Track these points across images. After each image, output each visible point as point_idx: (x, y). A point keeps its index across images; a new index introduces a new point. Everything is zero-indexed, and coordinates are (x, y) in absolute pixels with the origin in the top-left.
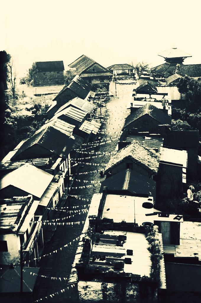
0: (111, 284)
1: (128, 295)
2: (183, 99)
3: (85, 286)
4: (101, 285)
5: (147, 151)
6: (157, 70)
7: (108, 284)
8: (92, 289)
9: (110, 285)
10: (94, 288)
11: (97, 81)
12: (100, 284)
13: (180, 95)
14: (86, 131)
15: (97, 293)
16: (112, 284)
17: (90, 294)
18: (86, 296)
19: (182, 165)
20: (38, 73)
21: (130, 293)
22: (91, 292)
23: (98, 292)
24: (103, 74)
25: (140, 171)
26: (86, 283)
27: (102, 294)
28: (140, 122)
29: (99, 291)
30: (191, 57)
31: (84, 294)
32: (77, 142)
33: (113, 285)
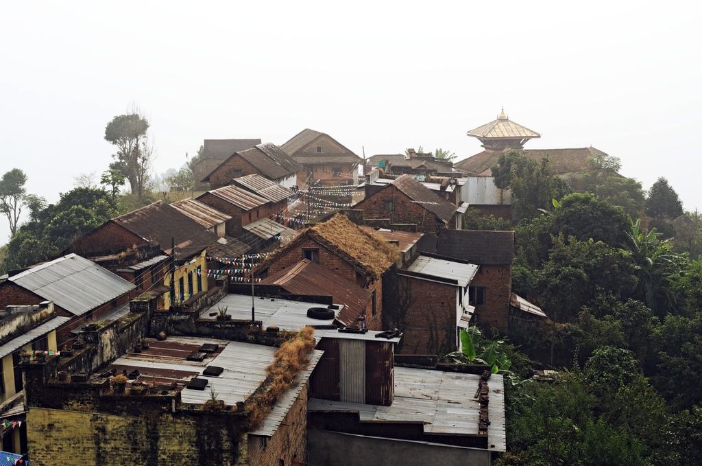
1: (164, 454)
3: (46, 423)
4: (91, 420)
6: (465, 165)
8: (65, 434)
9: (115, 423)
10: (70, 431)
11: (325, 174)
12: (88, 417)
13: (499, 195)
14: (259, 233)
16: (121, 419)
18: (49, 456)
19: (456, 282)
20: (205, 162)
22: (63, 443)
24: (339, 158)
25: (337, 269)
27: (92, 448)
28: (375, 203)
29: (85, 441)
30: (537, 139)
31: (43, 450)
33: (122, 424)
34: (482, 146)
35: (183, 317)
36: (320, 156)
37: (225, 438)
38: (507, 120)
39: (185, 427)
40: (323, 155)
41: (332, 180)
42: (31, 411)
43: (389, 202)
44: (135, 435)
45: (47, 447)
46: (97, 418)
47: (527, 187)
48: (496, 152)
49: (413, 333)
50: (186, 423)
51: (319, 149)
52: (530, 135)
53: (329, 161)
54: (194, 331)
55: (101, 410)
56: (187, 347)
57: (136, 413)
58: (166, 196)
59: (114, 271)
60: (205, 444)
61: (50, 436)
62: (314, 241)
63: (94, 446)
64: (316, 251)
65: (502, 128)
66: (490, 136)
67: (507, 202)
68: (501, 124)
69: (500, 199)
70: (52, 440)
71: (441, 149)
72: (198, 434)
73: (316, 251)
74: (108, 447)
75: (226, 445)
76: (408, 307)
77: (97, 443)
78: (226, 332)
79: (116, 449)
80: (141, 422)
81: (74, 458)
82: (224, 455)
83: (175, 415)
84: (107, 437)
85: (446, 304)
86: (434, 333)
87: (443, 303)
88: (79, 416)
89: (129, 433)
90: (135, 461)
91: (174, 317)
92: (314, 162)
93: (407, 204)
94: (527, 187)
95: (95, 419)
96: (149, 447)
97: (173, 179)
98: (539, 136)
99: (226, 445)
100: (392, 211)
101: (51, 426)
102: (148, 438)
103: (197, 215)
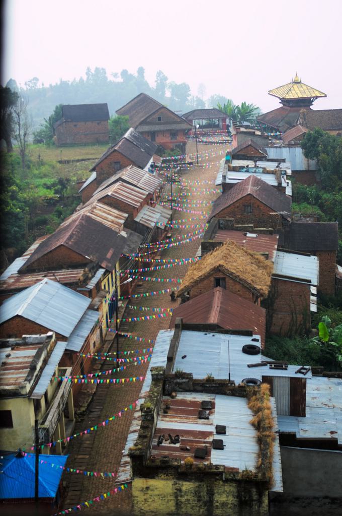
1: (217, 502)
3: (145, 486)
4: (173, 485)
8: (156, 492)
9: (187, 486)
10: (159, 491)
12: (170, 483)
15: (165, 500)
16: (191, 484)
18: (146, 505)
21: (222, 499)
24: (175, 125)
25: (239, 291)
26: (147, 482)
28: (238, 207)
31: (142, 501)
33: (191, 486)
34: (280, 103)
35: (184, 380)
36: (161, 124)
37: (254, 493)
38: (300, 82)
39: (230, 488)
40: (163, 124)
41: (171, 143)
42: (135, 480)
43: (248, 206)
44: (200, 492)
45: (145, 500)
46: (176, 484)
47: (331, 162)
48: (292, 109)
49: (279, 316)
50: (231, 486)
51: (159, 119)
52: (318, 95)
53: (168, 128)
54: (192, 389)
55: (178, 479)
56: (193, 404)
57: (202, 481)
58: (41, 158)
59: (75, 290)
60: (243, 497)
61: (147, 494)
62: (222, 272)
63: (174, 499)
64: (224, 279)
65: (297, 90)
66: (287, 97)
67: (312, 168)
68: (295, 86)
69: (307, 165)
70: (148, 496)
71: (245, 102)
72: (238, 491)
73: (224, 279)
74: (183, 499)
75: (255, 497)
76: (276, 299)
77: (176, 497)
78: (212, 389)
79: (188, 500)
80: (203, 485)
81: (162, 505)
82: (254, 503)
83: (224, 481)
84: (183, 494)
85: (303, 297)
86: (294, 316)
87: (301, 296)
88: (165, 482)
89: (196, 492)
90: (199, 507)
91: (178, 380)
92: (156, 129)
93: (261, 208)
94: (331, 162)
95: (175, 484)
96: (208, 499)
97: (36, 134)
98: (326, 96)
99: (255, 497)
100: (250, 212)
101: (147, 488)
102: (207, 494)
103: (106, 219)
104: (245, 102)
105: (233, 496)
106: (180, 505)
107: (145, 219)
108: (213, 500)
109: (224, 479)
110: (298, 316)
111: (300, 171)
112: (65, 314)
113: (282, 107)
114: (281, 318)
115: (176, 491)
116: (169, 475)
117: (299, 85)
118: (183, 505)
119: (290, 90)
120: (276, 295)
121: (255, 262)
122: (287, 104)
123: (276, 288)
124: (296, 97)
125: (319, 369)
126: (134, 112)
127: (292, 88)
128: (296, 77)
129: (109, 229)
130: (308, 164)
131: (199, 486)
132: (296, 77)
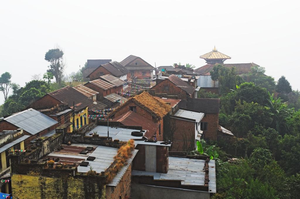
0: (50, 179)
1: (70, 194)
2: (216, 87)
3: (20, 181)
5: (157, 101)
7: (47, 178)
8: (28, 185)
9: (49, 181)
10: (30, 184)
12: (37, 178)
14: (111, 99)
15: (34, 191)
16: (52, 179)
17: (26, 192)
18: (21, 195)
19: (195, 120)
21: (74, 191)
22: (27, 189)
23: (35, 189)
25: (144, 115)
26: (21, 177)
27: (39, 191)
28: (160, 87)
29: (36, 188)
31: (18, 192)
32: (99, 106)
33: (52, 181)
34: (206, 62)
35: (78, 135)
36: (137, 66)
37: (96, 187)
38: (217, 51)
39: (79, 182)
42: (13, 175)
43: (166, 86)
44: (58, 186)
46: (42, 179)
50: (79, 181)
51: (136, 64)
53: (141, 69)
55: (43, 175)
57: (58, 176)
58: (71, 84)
59: (49, 116)
61: (21, 186)
63: (40, 190)
64: (135, 107)
65: (215, 55)
66: (209, 58)
68: (214, 53)
69: (214, 85)
70: (22, 188)
71: (188, 64)
72: (85, 185)
73: (135, 107)
74: (46, 191)
75: (97, 190)
77: (42, 189)
78: (97, 142)
79: (50, 192)
80: (60, 180)
82: (96, 194)
84: (46, 187)
86: (186, 142)
89: (55, 185)
90: (58, 197)
92: (134, 69)
98: (230, 58)
99: (97, 190)
100: (168, 90)
101: (22, 182)
103: (84, 92)
104: (188, 64)
105: (81, 189)
106: (44, 195)
107: (111, 98)
108: (67, 192)
109: (74, 175)
110: (188, 142)
111: (210, 88)
112: (37, 125)
113: (207, 65)
114: (177, 144)
115: (41, 184)
116: (37, 172)
117: (216, 53)
118: (46, 196)
119: (211, 55)
120: (174, 129)
121: (160, 104)
122: (209, 63)
123: (175, 125)
124: (214, 58)
125: (184, 153)
126: (152, 104)
127: (212, 54)
128: (215, 48)
129: (85, 96)
130: (214, 84)
131: (57, 181)
132: (215, 48)
